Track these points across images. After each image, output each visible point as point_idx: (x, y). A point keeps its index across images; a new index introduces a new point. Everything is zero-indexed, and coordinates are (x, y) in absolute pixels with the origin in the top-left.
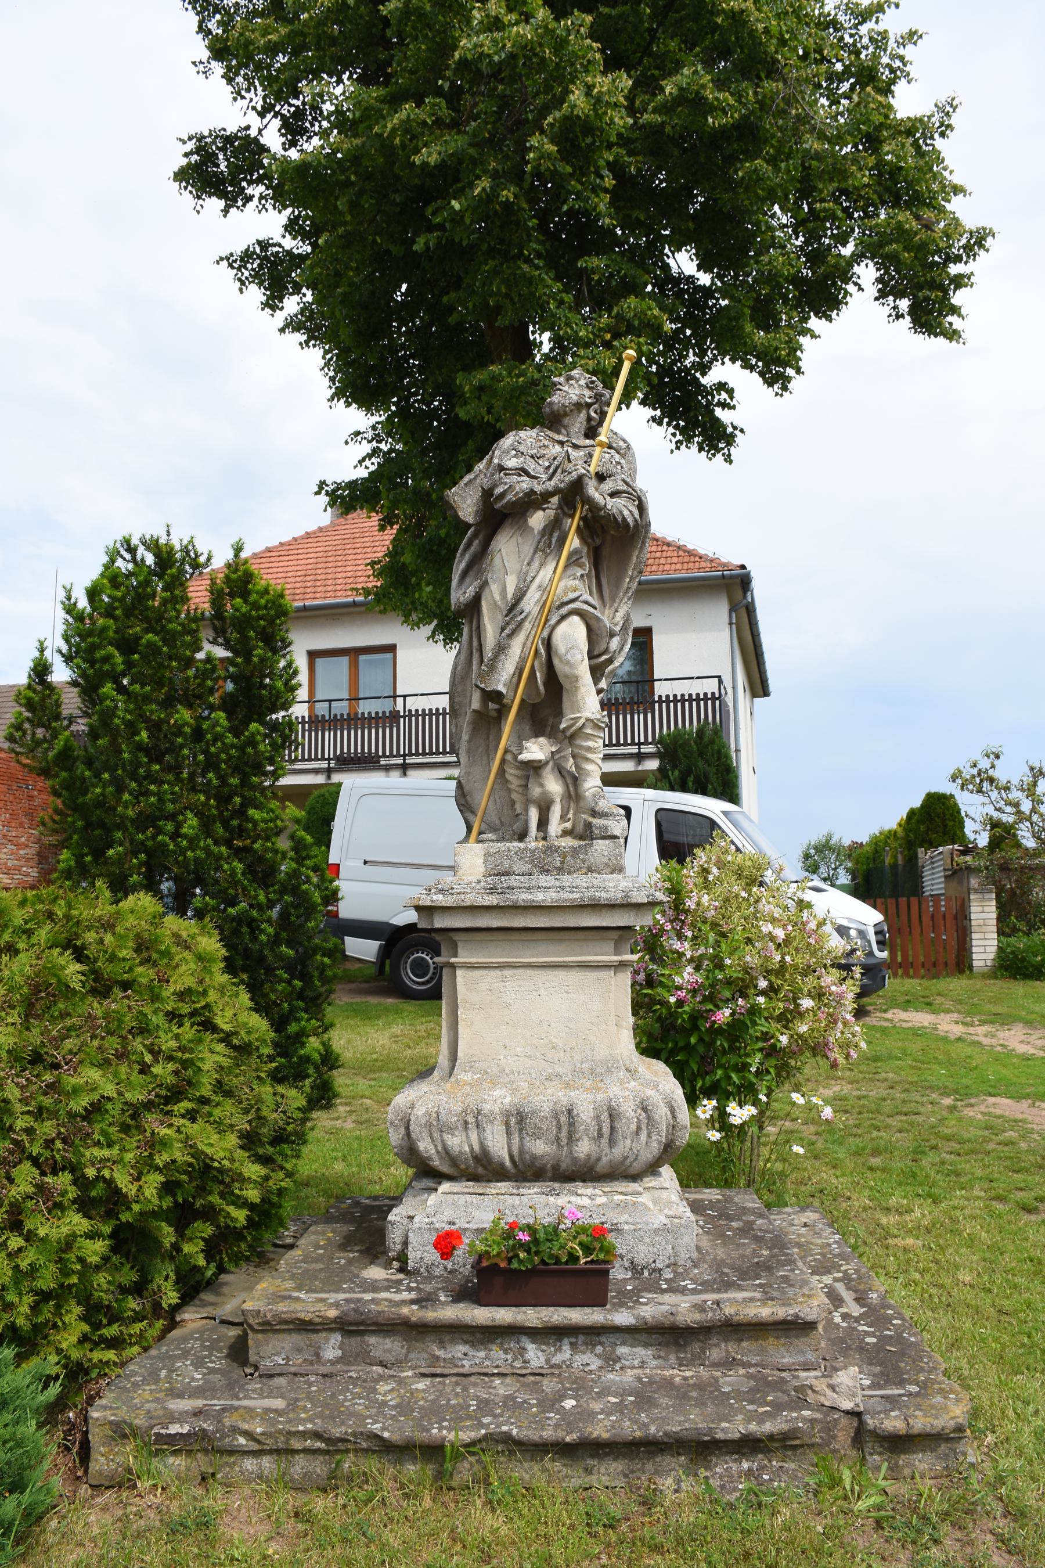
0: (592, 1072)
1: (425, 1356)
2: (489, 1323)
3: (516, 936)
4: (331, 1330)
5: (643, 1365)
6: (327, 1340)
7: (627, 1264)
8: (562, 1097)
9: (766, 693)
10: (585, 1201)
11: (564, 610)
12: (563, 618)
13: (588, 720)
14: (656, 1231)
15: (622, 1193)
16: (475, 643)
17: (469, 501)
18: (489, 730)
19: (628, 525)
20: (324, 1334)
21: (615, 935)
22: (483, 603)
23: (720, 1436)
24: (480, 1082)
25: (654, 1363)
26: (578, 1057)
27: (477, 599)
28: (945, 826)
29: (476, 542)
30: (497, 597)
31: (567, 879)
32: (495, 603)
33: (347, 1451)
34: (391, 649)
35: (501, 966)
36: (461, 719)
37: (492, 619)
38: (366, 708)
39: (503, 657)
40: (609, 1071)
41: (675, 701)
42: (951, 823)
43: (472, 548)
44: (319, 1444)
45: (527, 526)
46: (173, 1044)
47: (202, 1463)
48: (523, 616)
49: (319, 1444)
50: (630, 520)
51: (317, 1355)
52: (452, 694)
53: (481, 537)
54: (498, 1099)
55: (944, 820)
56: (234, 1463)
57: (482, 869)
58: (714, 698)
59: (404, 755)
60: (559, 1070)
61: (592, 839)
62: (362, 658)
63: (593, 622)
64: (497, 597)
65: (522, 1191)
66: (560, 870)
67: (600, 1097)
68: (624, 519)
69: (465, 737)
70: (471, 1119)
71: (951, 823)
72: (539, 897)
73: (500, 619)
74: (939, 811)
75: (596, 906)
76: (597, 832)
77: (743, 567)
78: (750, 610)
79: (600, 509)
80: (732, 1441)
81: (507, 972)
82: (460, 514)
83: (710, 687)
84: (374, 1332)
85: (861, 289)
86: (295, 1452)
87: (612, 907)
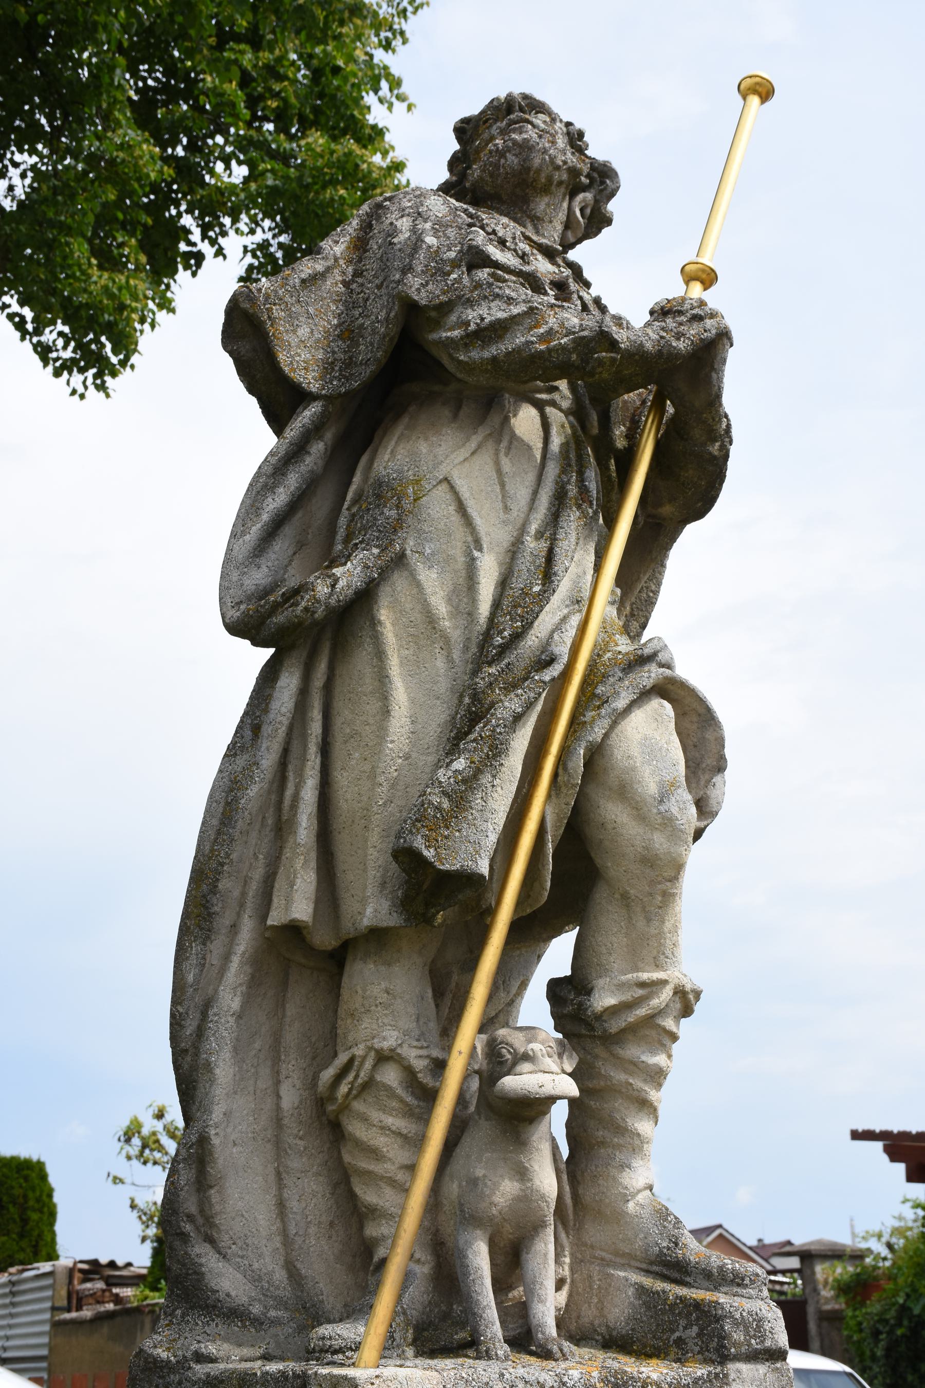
16: (316, 728)
17: (303, 331)
18: (284, 985)
22: (384, 615)
27: (364, 599)
28: (25, 1221)
29: (318, 448)
30: (440, 606)
32: (431, 619)
36: (216, 947)
37: (413, 667)
42: (35, 1216)
43: (308, 460)
45: (513, 436)
48: (555, 670)
53: (329, 435)
55: (23, 1209)
61: (724, 1358)
64: (440, 606)
69: (230, 999)
71: (35, 1216)
73: (442, 672)
74: (17, 1192)
76: (738, 1336)
82: (282, 357)
85: (220, 252)
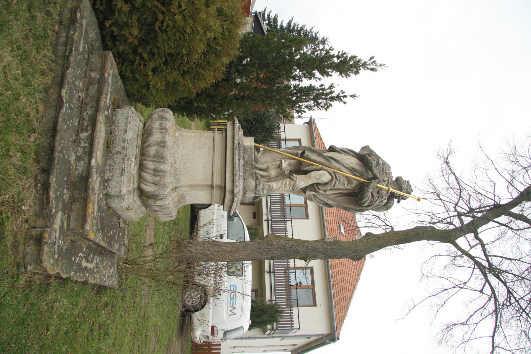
0: (177, 174)
1: (89, 101)
2: (93, 150)
3: (224, 152)
4: (101, 75)
5: (76, 169)
6: (98, 74)
7: (110, 178)
8: (170, 160)
9: (308, 219)
10: (132, 168)
11: (333, 174)
12: (330, 174)
13: (296, 182)
14: (120, 188)
15: (134, 180)
19: (362, 199)
20: (99, 73)
21: (223, 185)
23: (51, 177)
24: (175, 138)
25: (76, 173)
26: (181, 170)
31: (242, 168)
33: (64, 61)
34: (307, 217)
35: (213, 147)
38: (287, 210)
39: (316, 154)
40: (176, 180)
41: (291, 318)
44: (67, 54)
46: (153, 332)
47: (66, 22)
49: (67, 54)
50: (364, 200)
51: (93, 71)
52: (292, 239)
54: (169, 139)
56: (65, 30)
57: (246, 145)
58: (292, 327)
59: (271, 220)
60: (178, 164)
62: (304, 208)
63: (329, 184)
65: (138, 148)
66: (245, 169)
67: (168, 174)
68: (364, 197)
70: (164, 131)
72: (237, 157)
75: (233, 175)
77: (338, 339)
78: (323, 344)
79: (368, 187)
80: (49, 180)
81: (212, 149)
83: (296, 326)
84: (99, 86)
86: (66, 46)
87: (233, 181)
